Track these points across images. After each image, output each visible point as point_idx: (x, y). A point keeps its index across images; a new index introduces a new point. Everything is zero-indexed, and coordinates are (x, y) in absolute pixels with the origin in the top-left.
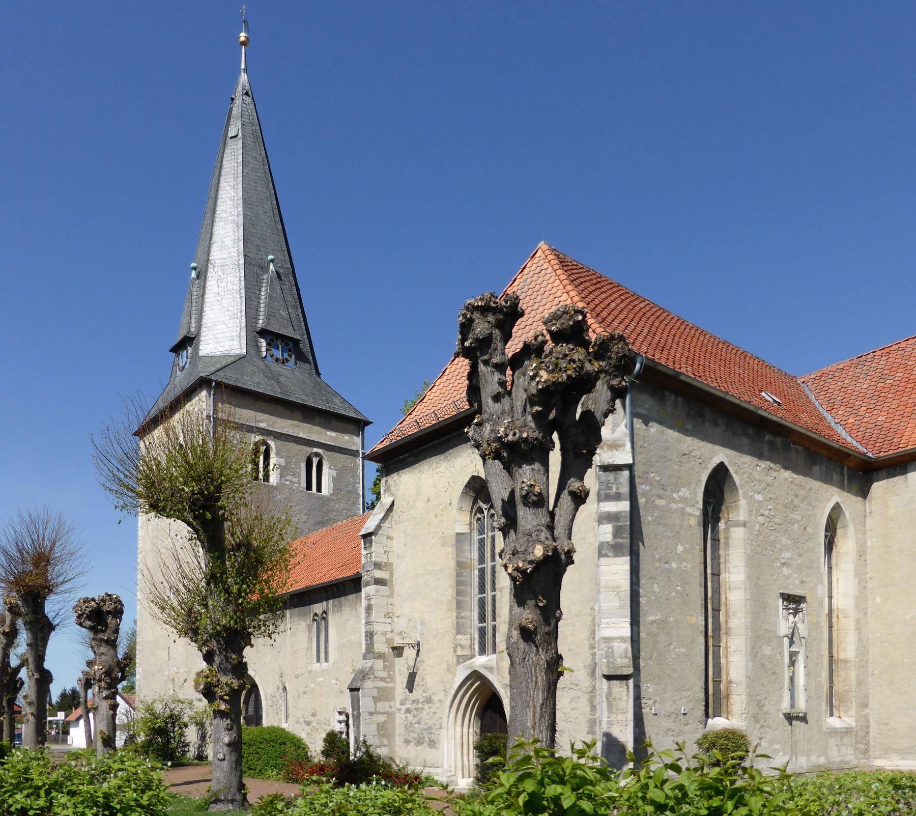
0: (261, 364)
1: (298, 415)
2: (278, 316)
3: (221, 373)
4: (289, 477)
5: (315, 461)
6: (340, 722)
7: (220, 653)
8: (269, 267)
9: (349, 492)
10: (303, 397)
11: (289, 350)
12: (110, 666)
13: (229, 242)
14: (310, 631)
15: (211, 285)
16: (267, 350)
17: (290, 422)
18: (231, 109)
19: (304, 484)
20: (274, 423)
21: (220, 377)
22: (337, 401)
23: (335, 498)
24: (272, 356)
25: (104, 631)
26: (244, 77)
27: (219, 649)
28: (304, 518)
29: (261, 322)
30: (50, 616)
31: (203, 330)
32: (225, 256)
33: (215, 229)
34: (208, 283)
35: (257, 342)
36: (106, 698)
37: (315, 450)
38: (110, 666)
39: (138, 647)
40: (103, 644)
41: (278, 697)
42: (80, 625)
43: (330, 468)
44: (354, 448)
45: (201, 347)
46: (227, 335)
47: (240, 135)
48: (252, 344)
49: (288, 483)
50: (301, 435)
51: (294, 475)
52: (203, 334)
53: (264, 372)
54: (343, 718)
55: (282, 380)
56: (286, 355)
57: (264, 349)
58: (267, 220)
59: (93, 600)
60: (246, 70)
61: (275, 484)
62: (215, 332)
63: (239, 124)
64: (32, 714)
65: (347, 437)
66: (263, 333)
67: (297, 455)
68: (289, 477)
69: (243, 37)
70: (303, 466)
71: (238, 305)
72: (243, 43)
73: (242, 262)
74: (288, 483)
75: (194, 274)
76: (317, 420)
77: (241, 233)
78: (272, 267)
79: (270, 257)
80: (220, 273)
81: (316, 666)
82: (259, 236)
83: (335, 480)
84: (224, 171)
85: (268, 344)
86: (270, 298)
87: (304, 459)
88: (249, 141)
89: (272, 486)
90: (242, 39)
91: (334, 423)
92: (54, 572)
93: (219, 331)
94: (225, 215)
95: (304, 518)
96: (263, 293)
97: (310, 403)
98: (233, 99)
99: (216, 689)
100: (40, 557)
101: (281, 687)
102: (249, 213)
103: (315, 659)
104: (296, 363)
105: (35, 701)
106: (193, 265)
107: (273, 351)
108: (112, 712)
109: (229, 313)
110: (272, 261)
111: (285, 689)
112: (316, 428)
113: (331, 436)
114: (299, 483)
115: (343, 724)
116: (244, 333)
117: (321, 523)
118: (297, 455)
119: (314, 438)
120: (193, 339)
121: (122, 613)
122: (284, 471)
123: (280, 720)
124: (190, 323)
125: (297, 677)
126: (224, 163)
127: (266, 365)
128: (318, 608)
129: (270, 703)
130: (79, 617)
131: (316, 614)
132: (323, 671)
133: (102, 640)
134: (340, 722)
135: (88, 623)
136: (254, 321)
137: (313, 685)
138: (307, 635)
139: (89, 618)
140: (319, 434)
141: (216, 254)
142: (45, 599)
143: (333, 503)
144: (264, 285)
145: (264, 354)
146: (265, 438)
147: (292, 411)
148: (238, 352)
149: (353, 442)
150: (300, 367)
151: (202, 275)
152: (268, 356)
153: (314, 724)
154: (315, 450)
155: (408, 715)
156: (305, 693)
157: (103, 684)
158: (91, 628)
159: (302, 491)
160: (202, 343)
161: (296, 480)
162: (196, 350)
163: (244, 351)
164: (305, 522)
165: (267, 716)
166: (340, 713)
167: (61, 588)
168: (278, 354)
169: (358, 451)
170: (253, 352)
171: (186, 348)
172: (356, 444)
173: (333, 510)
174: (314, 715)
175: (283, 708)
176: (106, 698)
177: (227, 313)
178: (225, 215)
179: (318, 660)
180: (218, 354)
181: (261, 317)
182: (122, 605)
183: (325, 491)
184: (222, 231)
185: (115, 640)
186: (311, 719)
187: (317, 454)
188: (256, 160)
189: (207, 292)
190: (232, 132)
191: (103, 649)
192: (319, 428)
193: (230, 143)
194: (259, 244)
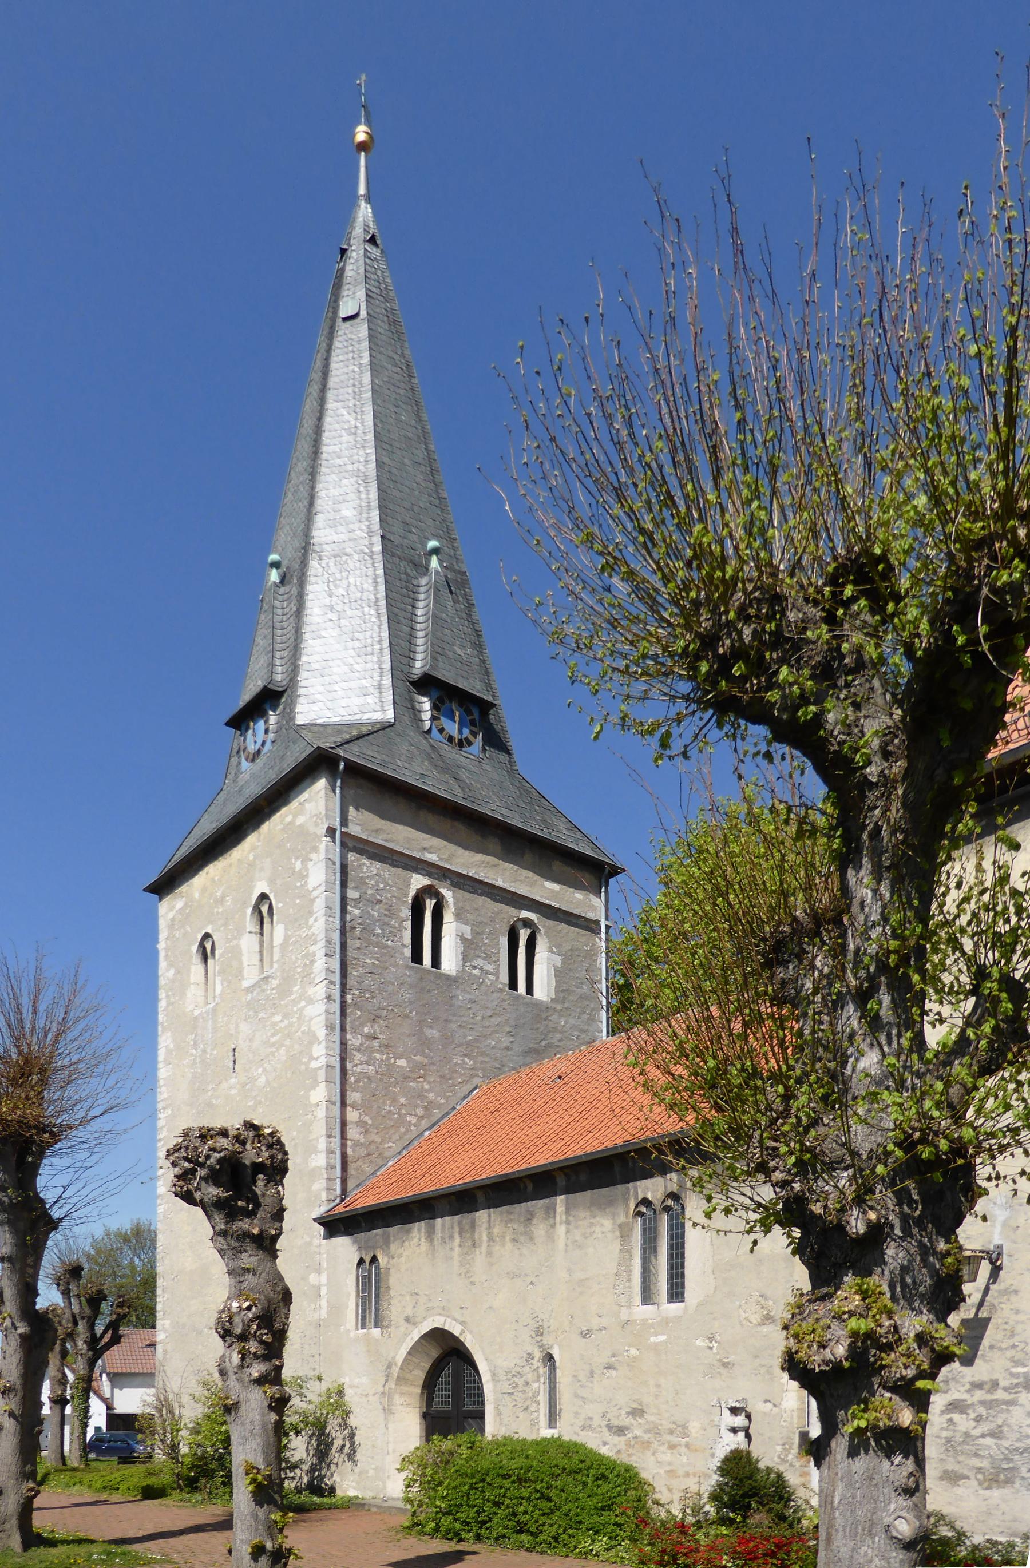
0: (419, 739)
1: (493, 843)
2: (450, 654)
3: (354, 747)
4: (479, 962)
5: (524, 935)
6: (734, 1430)
7: (907, 1233)
8: (428, 562)
9: (582, 997)
10: (504, 811)
11: (473, 723)
12: (269, 1301)
13: (348, 512)
14: (625, 1235)
15: (316, 591)
16: (433, 718)
17: (479, 857)
18: (342, 270)
19: (504, 978)
20: (451, 856)
21: (353, 754)
22: (562, 826)
23: (559, 1007)
24: (441, 731)
25: (251, 1214)
26: (364, 211)
27: (904, 1219)
28: (505, 1041)
29: (418, 664)
30: (48, 1196)
31: (303, 675)
32: (343, 537)
33: (319, 486)
34: (309, 588)
35: (412, 701)
36: (260, 1381)
37: (525, 914)
38: (269, 1301)
39: (159, 1282)
40: (249, 1247)
41: (530, 1377)
42: (188, 1197)
43: (550, 951)
44: (592, 916)
45: (299, 708)
46: (353, 685)
47: (363, 313)
48: (404, 705)
49: (476, 972)
50: (500, 883)
51: (488, 958)
52: (303, 683)
53: (429, 758)
54: (740, 1421)
55: (464, 775)
56: (466, 732)
57: (426, 716)
58: (420, 478)
59: (224, 1133)
60: (368, 199)
61: (454, 973)
62: (327, 679)
63: (361, 294)
64: (11, 1414)
65: (579, 895)
66: (426, 684)
67: (493, 920)
68: (479, 962)
69: (361, 134)
70: (504, 941)
71: (375, 630)
72: (362, 146)
73: (378, 548)
74: (476, 972)
75: (274, 576)
76: (528, 857)
77: (374, 495)
78: (434, 563)
79: (432, 544)
80: (333, 569)
81: (643, 1312)
82: (407, 504)
83: (560, 974)
84: (332, 382)
85: (435, 707)
86: (437, 620)
87: (506, 929)
88: (382, 328)
89: (448, 977)
90: (361, 136)
91: (558, 866)
92: (60, 1101)
93: (336, 678)
94: (338, 461)
95: (505, 1041)
96: (419, 612)
97: (516, 821)
98: (343, 251)
99: (889, 1358)
100: (27, 1062)
101: (538, 1355)
102: (386, 460)
103: (638, 1298)
104: (484, 750)
105: (18, 1386)
106: (274, 557)
107: (444, 722)
108: (273, 1417)
109: (357, 644)
110: (435, 551)
111: (550, 1358)
112: (526, 873)
113: (552, 891)
114: (497, 974)
115: (741, 1435)
116: (387, 681)
117: (537, 1053)
118: (493, 920)
119: (523, 890)
120: (279, 695)
121: (285, 1170)
122: (469, 948)
123: (534, 1423)
124: (273, 665)
125: (585, 1334)
126: (333, 366)
127: (432, 746)
128: (654, 1188)
129: (506, 1387)
130: (184, 1176)
131: (646, 1202)
132: (665, 1322)
133: (246, 1236)
134: (734, 1430)
135: (213, 1191)
136: (405, 661)
137: (634, 1352)
138: (617, 1245)
139: (213, 1178)
140: (532, 884)
141: (322, 534)
142: (41, 1155)
143: (555, 1016)
144: (422, 596)
145: (427, 725)
146: (436, 883)
147: (483, 836)
148: (377, 716)
149: (590, 904)
150: (491, 758)
151: (295, 577)
152: (435, 731)
153: (638, 1432)
154: (525, 914)
155: (956, 1417)
156: (609, 1367)
157: (253, 1346)
158: (220, 1205)
159: (501, 990)
160: (301, 700)
161: (490, 968)
162: (289, 716)
163: (390, 715)
164: (507, 1048)
165: (499, 1414)
166: (734, 1411)
167: (80, 1133)
168: (453, 728)
169: (597, 922)
170: (406, 719)
171: (263, 714)
172: (594, 908)
173: (555, 1030)
174: (637, 1412)
175: (543, 1398)
176: (260, 1381)
177: (351, 644)
178: (338, 461)
179: (647, 1296)
180: (335, 720)
181: (419, 656)
182: (286, 1153)
183: (541, 992)
184: (334, 492)
185: (275, 1238)
186: (628, 1421)
187: (527, 923)
188: (396, 365)
189: (308, 604)
190: (346, 308)
191: (249, 1259)
192: (531, 874)
193: (343, 330)
194: (408, 520)
